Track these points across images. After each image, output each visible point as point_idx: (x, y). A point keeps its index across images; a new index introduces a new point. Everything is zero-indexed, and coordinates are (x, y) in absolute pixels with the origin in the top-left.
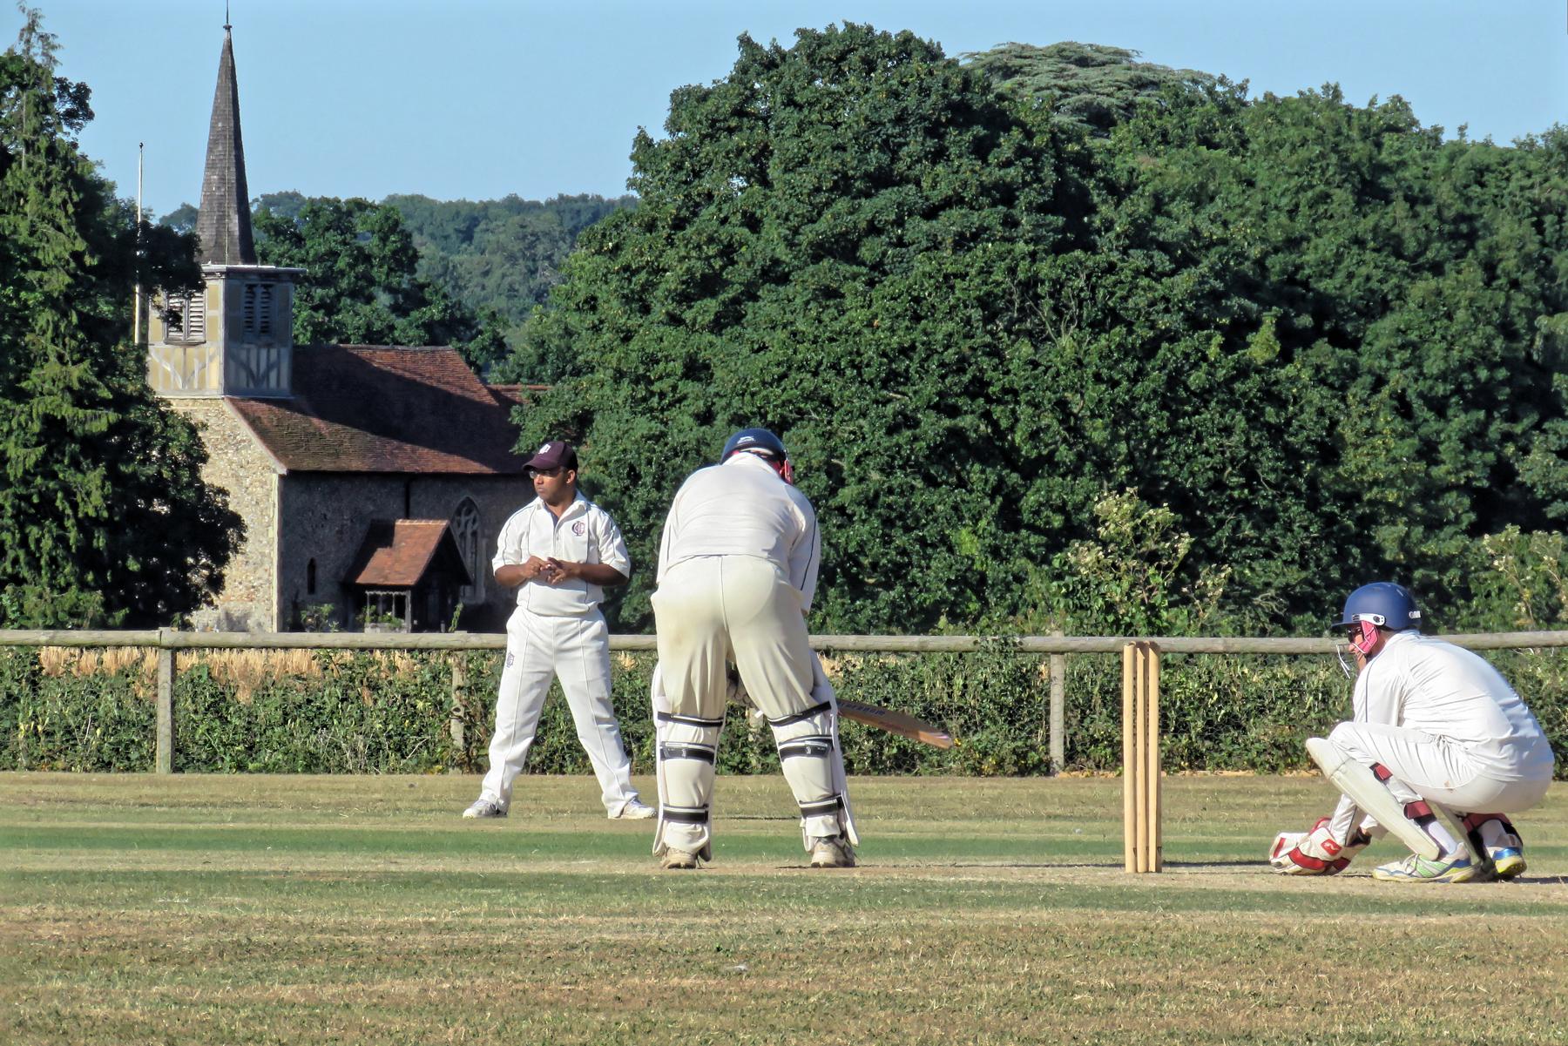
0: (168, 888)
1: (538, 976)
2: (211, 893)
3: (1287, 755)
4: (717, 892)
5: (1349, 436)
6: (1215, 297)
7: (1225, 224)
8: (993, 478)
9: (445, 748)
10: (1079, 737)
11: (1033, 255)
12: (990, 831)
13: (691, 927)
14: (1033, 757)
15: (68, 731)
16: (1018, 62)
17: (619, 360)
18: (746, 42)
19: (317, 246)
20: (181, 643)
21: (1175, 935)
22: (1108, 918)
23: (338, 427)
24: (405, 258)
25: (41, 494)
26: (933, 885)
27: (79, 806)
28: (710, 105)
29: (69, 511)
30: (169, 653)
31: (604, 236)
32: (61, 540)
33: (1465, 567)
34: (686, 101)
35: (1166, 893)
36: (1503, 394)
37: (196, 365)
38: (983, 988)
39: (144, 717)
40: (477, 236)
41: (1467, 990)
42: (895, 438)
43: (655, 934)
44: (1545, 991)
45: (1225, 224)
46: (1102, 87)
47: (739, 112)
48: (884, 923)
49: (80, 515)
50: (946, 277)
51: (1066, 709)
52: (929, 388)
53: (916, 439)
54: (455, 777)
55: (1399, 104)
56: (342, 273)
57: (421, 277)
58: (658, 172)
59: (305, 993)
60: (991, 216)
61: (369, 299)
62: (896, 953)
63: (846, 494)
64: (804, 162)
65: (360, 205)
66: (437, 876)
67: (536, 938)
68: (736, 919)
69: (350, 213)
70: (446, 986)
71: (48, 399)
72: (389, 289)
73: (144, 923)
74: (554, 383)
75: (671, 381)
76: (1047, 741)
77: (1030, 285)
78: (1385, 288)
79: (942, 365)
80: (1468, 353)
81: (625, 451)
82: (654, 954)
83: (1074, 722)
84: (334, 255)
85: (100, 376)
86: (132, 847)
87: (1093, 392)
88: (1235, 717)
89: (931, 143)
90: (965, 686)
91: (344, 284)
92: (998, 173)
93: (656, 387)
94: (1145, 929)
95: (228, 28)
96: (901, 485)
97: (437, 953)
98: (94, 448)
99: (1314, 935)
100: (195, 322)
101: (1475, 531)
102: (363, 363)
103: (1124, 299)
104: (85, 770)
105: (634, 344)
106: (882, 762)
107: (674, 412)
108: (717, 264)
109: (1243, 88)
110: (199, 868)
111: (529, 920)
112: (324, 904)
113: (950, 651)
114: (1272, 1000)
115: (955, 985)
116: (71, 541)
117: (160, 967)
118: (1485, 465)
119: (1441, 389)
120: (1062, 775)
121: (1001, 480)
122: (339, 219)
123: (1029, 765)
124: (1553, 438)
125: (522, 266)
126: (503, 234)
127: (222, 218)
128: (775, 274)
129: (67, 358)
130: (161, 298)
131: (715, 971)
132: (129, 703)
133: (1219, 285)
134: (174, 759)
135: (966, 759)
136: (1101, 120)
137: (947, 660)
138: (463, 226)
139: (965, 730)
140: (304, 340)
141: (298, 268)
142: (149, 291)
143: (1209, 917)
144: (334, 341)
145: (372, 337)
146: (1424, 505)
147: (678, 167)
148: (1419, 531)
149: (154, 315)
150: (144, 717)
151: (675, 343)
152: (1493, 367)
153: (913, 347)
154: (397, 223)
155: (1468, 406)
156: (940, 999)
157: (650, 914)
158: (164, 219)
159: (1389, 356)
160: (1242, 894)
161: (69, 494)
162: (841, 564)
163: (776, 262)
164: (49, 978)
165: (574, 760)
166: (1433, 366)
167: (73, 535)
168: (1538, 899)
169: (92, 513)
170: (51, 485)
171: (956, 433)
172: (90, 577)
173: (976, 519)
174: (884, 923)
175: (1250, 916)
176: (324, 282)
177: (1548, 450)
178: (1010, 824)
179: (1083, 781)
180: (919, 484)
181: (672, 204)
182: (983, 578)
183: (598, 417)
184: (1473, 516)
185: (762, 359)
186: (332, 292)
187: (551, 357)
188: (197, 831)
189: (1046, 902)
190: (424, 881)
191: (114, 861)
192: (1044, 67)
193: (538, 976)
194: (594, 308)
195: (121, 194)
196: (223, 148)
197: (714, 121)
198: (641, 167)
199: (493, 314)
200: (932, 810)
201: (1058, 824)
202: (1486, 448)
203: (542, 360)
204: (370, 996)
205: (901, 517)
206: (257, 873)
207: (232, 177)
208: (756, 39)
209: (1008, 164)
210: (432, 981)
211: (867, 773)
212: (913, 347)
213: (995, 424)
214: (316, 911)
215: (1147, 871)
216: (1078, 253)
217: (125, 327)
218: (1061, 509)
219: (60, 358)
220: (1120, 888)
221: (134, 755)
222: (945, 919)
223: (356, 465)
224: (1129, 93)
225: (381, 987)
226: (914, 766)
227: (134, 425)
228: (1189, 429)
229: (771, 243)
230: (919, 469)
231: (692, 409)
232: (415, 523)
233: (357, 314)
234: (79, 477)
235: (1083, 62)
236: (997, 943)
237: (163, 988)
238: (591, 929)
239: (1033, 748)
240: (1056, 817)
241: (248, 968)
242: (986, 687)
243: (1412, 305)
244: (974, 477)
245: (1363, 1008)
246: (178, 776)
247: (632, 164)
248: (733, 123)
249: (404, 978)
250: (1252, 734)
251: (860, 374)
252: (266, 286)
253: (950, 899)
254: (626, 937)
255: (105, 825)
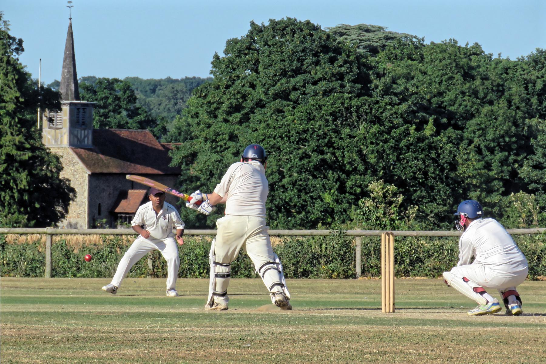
0: (49, 318)
1: (178, 348)
2: (64, 319)
3: (438, 272)
4: (240, 319)
5: (460, 161)
6: (414, 112)
7: (417, 87)
8: (336, 176)
9: (146, 269)
10: (366, 265)
11: (350, 98)
12: (335, 298)
13: (231, 331)
14: (350, 272)
15: (15, 263)
16: (345, 31)
17: (206, 134)
18: (253, 24)
19: (101, 95)
20: (54, 233)
21: (399, 334)
22: (376, 328)
23: (108, 157)
24: (132, 99)
25: (5, 181)
26: (315, 317)
27: (18, 289)
28: (238, 45)
29: (15, 187)
30: (50, 236)
31: (201, 91)
32: (12, 197)
33: (500, 206)
34: (232, 44)
35: (396, 320)
36: (514, 146)
37: (59, 136)
38: (333, 353)
39: (41, 258)
40: (157, 91)
41: (501, 353)
42: (303, 162)
43: (219, 334)
44: (528, 354)
45: (417, 87)
46: (374, 40)
47: (249, 48)
48: (298, 330)
49: (19, 188)
50: (319, 106)
51: (361, 256)
52: (313, 144)
53: (310, 162)
54: (149, 279)
55: (477, 46)
56: (110, 104)
57: (137, 105)
58: (220, 68)
59: (97, 354)
60: (336, 84)
61: (120, 113)
62: (302, 340)
63: (285, 181)
64: (271, 65)
65: (116, 81)
66: (143, 313)
67: (177, 335)
68: (247, 329)
69: (113, 83)
70: (146, 351)
71: (8, 148)
72: (126, 110)
73: (41, 330)
74: (184, 142)
75: (224, 141)
76: (355, 267)
77: (348, 109)
78: (473, 109)
79: (318, 136)
80: (502, 132)
81: (208, 166)
82: (218, 341)
83: (364, 260)
84: (107, 98)
85: (26, 140)
86: (37, 303)
87: (371, 147)
88: (420, 258)
89: (315, 59)
90: (326, 248)
91: (111, 108)
92: (338, 69)
93: (219, 144)
94: (389, 332)
95: (70, 19)
96: (304, 178)
97: (143, 340)
98: (24, 165)
99: (448, 334)
100: (59, 121)
101: (506, 194)
102: (118, 136)
103: (382, 113)
104: (21, 276)
105: (212, 129)
106: (297, 274)
107: (226, 152)
108: (241, 101)
109: (423, 40)
110: (60, 311)
111: (175, 329)
112: (103, 323)
113: (321, 236)
114: (433, 357)
115: (323, 352)
116: (16, 197)
117: (47, 345)
118: (508, 171)
119: (492, 145)
120: (360, 278)
121: (339, 177)
122: (109, 85)
123: (349, 275)
124: (530, 161)
125: (173, 101)
126: (167, 91)
127: (68, 85)
128: (260, 104)
129: (14, 133)
130: (47, 113)
131: (239, 347)
132: (36, 253)
133: (415, 108)
134: (52, 273)
135: (327, 273)
136: (374, 51)
137: (320, 238)
138: (152, 88)
139: (327, 263)
140: (97, 127)
141: (95, 102)
142: (43, 110)
143: (409, 328)
144: (107, 128)
145: (120, 126)
146: (486, 185)
147: (227, 67)
148: (484, 194)
149: (44, 119)
150: (41, 258)
151: (225, 128)
152: (511, 137)
153: (308, 130)
154: (129, 86)
155: (502, 150)
156: (318, 357)
157: (217, 327)
158: (48, 85)
159: (474, 133)
160: (422, 320)
161: (15, 181)
162: (283, 205)
163: (261, 100)
164: (8, 349)
165: (191, 273)
166: (490, 136)
167: (16, 195)
168: (525, 322)
169: (23, 187)
170: (9, 178)
171: (324, 161)
172: (22, 209)
173: (330, 190)
174: (298, 330)
175: (426, 328)
176: (105, 107)
177: (529, 166)
178: (342, 295)
179: (367, 281)
180: (311, 177)
181: (225, 80)
182: (333, 209)
183: (199, 154)
184: (503, 189)
185: (255, 134)
186: (107, 111)
187: (183, 133)
188: (59, 298)
189: (354, 323)
190: (139, 315)
191: (31, 308)
192: (354, 32)
193: (178, 348)
194: (197, 117)
195: (34, 77)
196: (69, 61)
197: (240, 51)
198: (215, 67)
199: (163, 118)
200: (314, 290)
201: (359, 296)
202: (508, 165)
203: (180, 134)
204: (119, 355)
205: (305, 189)
206: (80, 312)
207: (72, 71)
208: (256, 23)
209: (341, 66)
210: (141, 350)
211: (292, 278)
212: (308, 130)
213: (335, 156)
214: (101, 326)
215: (390, 312)
216: (366, 97)
217: (34, 122)
218: (360, 186)
219: (12, 134)
220: (380, 318)
221: (38, 271)
222: (319, 328)
223: (115, 171)
224: (384, 42)
225: (124, 352)
226: (309, 275)
227: (38, 157)
228: (404, 159)
229: (259, 93)
230: (310, 172)
231: (232, 151)
232: (136, 191)
233: (115, 118)
234: (19, 175)
235: (368, 31)
236: (338, 337)
237: (47, 353)
238: (196, 332)
239: (350, 269)
240: (358, 293)
241: (77, 345)
242: (334, 248)
243: (482, 115)
244: (330, 176)
245: (465, 360)
246: (53, 279)
247: (212, 65)
248: (246, 52)
249: (131, 349)
250: (426, 265)
251: (289, 139)
252: (84, 109)
253: (321, 322)
254: (208, 335)
255: (28, 295)
